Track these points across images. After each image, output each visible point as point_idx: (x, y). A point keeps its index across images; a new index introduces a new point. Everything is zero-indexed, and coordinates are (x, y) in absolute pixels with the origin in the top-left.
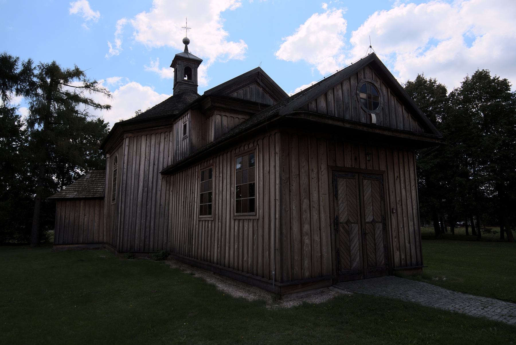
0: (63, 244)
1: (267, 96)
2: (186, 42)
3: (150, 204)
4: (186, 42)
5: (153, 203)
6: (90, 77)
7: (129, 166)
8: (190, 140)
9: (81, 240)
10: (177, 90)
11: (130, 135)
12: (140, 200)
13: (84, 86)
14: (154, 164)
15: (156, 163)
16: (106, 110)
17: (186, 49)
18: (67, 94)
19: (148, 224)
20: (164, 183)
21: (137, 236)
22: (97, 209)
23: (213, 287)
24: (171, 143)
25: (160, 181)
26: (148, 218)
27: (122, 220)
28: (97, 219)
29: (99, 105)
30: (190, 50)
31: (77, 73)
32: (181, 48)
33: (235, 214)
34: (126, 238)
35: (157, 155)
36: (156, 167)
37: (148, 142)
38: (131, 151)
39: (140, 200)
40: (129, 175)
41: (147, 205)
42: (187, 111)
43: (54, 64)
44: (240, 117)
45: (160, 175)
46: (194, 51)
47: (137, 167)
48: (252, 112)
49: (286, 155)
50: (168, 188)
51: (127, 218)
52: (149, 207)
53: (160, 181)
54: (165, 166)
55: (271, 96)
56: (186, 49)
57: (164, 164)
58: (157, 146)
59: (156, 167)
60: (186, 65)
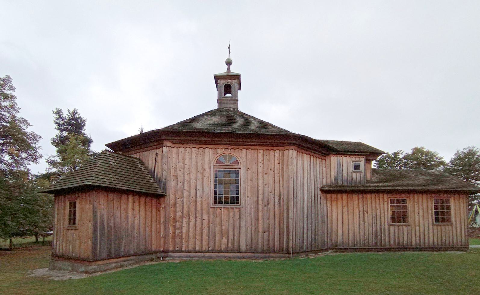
17: (229, 69)
33: (435, 223)
56: (229, 69)
60: (228, 84)
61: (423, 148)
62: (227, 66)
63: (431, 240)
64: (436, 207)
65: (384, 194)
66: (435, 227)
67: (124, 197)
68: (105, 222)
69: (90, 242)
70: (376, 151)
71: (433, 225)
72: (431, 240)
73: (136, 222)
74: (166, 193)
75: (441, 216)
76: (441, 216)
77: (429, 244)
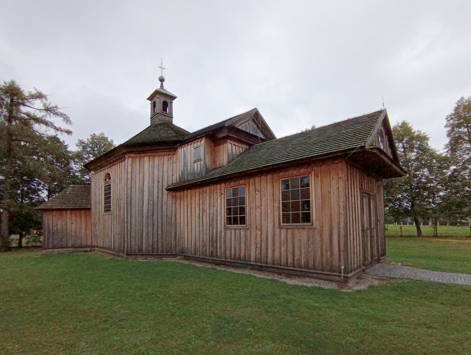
0: (53, 248)
1: (259, 131)
2: (162, 80)
3: (156, 215)
4: (162, 80)
5: (160, 214)
6: (52, 102)
7: (133, 183)
8: (205, 163)
9: (70, 245)
10: (153, 122)
11: (132, 155)
12: (145, 211)
13: (44, 109)
14: (158, 182)
15: (160, 180)
16: (66, 134)
17: (162, 86)
18: (28, 115)
19: (155, 230)
20: (170, 197)
21: (144, 241)
22: (83, 218)
23: (285, 283)
24: (174, 164)
25: (165, 196)
26: (155, 226)
27: (129, 228)
28: (84, 226)
29: (60, 128)
30: (165, 87)
31: (40, 96)
32: (157, 86)
33: (282, 224)
34: (133, 243)
35: (161, 174)
36: (160, 184)
37: (151, 164)
38: (134, 169)
39: (145, 211)
40: (133, 190)
41: (153, 216)
42: (202, 137)
43: (13, 83)
44: (244, 146)
45: (165, 191)
46: (169, 88)
47: (141, 183)
48: (251, 143)
49: (361, 178)
50: (174, 202)
51: (133, 226)
52: (155, 217)
53: (165, 196)
54: (170, 183)
55: (261, 131)
56: (162, 86)
57: (169, 182)
58: (161, 166)
59: (160, 184)
60: (162, 101)
61: (462, 98)
62: (160, 83)
63: (277, 254)
64: (285, 196)
65: (221, 184)
66: (283, 232)
67: (64, 212)
68: (51, 228)
69: (243, 232)
70: (242, 116)
71: (280, 227)
72: (277, 254)
73: (73, 227)
74: (91, 206)
75: (297, 211)
76: (297, 211)
77: (274, 261)
